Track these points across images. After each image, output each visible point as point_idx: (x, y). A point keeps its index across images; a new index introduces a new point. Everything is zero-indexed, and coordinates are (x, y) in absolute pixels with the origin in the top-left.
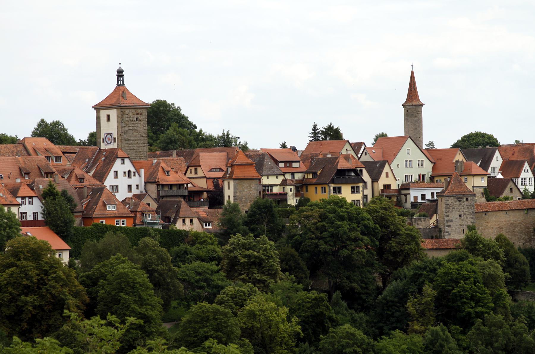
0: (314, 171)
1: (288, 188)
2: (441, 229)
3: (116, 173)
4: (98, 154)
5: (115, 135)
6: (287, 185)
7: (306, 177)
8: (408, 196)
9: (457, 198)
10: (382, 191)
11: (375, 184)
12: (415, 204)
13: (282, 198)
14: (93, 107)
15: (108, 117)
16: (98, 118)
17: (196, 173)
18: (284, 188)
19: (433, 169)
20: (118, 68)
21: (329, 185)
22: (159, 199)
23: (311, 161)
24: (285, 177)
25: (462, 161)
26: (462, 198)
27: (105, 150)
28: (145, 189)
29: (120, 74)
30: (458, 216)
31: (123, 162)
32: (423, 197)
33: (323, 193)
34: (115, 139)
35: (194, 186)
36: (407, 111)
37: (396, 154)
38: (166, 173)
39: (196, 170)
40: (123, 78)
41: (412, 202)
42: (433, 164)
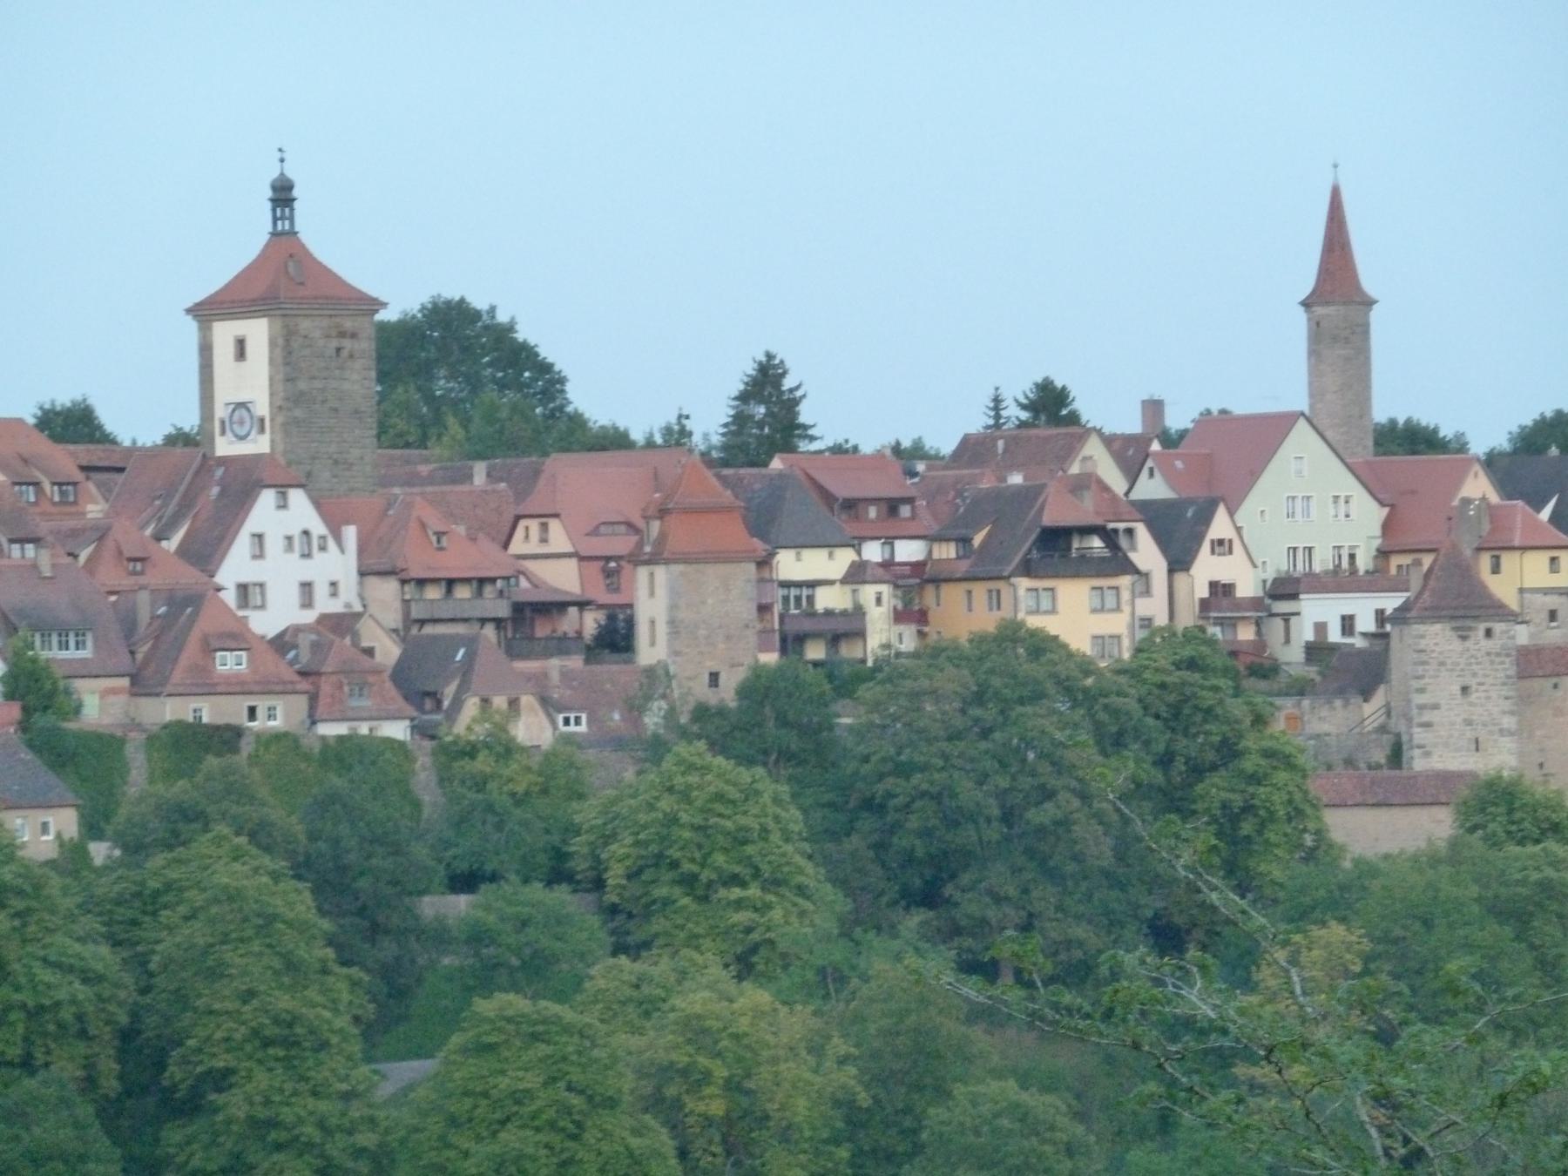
0: (963, 532)
1: (868, 592)
2: (1398, 735)
3: (259, 537)
4: (197, 473)
5: (262, 408)
6: (864, 582)
7: (936, 556)
8: (1293, 620)
9: (1456, 629)
10: (1205, 605)
11: (1180, 578)
12: (1317, 650)
13: (849, 627)
14: (189, 311)
15: (241, 344)
16: (206, 350)
17: (544, 540)
18: (854, 591)
19: (1387, 527)
20: (275, 174)
21: (1013, 580)
22: (407, 628)
23: (955, 499)
24: (859, 553)
25: (1484, 499)
26: (1470, 629)
27: (224, 461)
28: (362, 597)
29: (283, 195)
30: (1459, 692)
31: (283, 505)
32: (1348, 623)
33: (991, 609)
34: (262, 420)
35: (536, 586)
36: (1318, 324)
37: (1254, 474)
38: (434, 539)
39: (544, 527)
40: (292, 210)
41: (1307, 643)
42: (1386, 510)
